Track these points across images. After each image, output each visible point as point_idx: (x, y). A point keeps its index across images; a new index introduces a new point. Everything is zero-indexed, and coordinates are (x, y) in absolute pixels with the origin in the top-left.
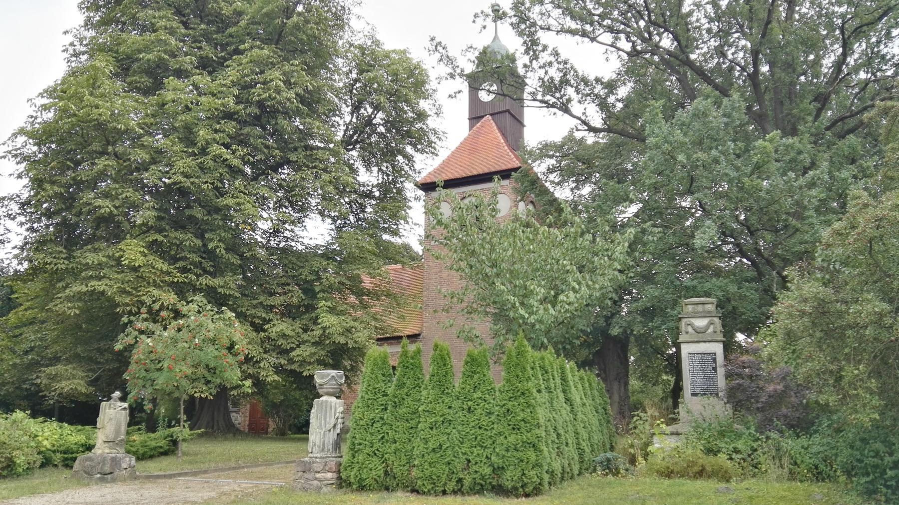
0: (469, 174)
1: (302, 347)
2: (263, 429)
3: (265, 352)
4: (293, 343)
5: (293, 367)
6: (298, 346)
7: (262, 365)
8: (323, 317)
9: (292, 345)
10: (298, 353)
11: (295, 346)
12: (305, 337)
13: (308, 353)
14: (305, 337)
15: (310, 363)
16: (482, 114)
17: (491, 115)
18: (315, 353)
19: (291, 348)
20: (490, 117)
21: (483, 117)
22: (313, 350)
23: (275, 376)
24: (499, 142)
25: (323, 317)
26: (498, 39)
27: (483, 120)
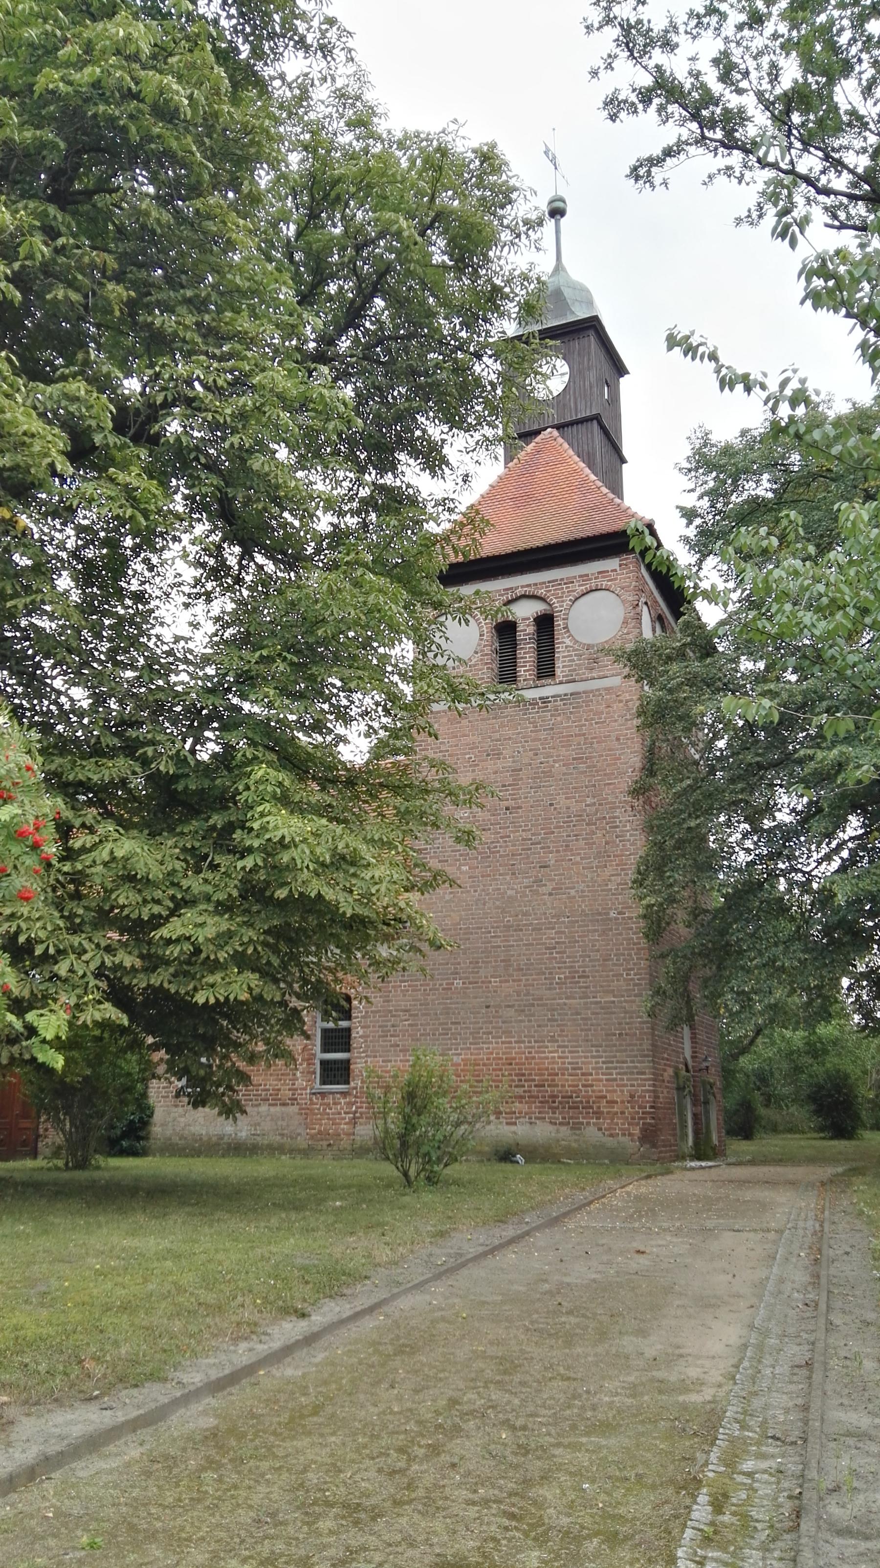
0: (522, 546)
1: (189, 914)
2: (25, 1144)
3: (75, 929)
4: (158, 902)
5: (155, 980)
6: (173, 913)
7: (62, 969)
8: (262, 815)
9: (157, 909)
10: (180, 931)
11: (165, 913)
12: (195, 884)
13: (210, 932)
14: (195, 884)
15: (214, 966)
16: (536, 427)
17: (559, 427)
18: (229, 935)
19: (153, 916)
20: (555, 433)
21: (537, 432)
22: (224, 924)
23: (107, 1005)
24: (586, 480)
25: (262, 815)
26: (564, 270)
27: (538, 439)
